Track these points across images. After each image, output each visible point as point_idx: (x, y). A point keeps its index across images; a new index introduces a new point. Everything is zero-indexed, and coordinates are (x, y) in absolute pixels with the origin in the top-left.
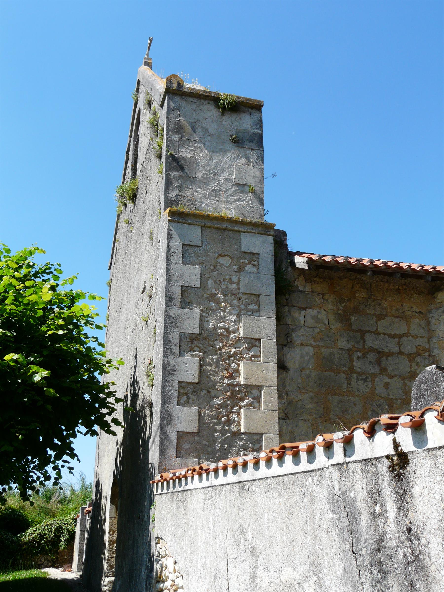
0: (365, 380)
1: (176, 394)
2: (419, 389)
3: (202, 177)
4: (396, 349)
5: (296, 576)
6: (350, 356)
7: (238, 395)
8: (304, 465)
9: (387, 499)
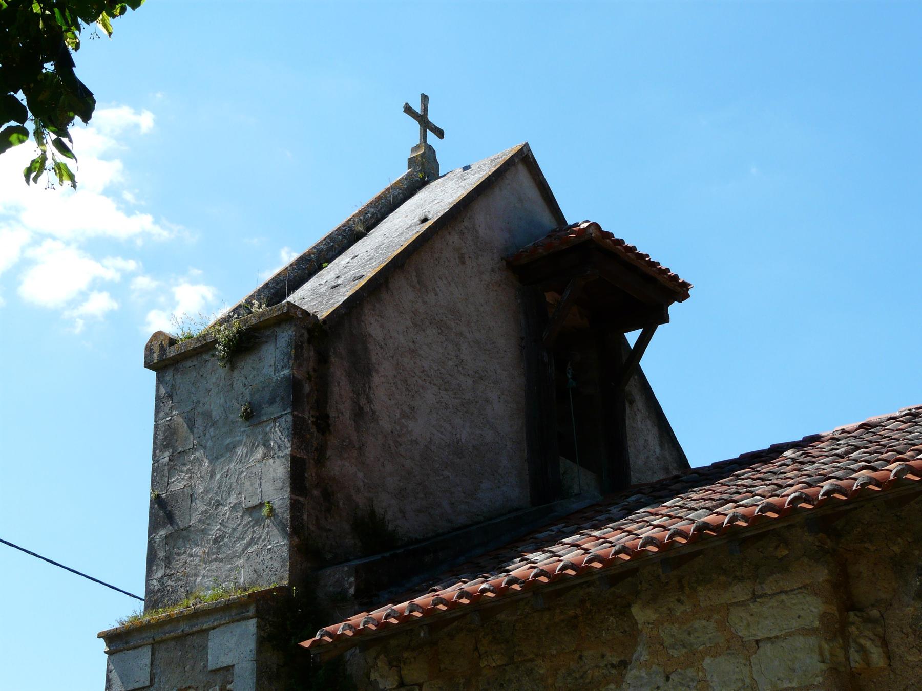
3: (200, 521)
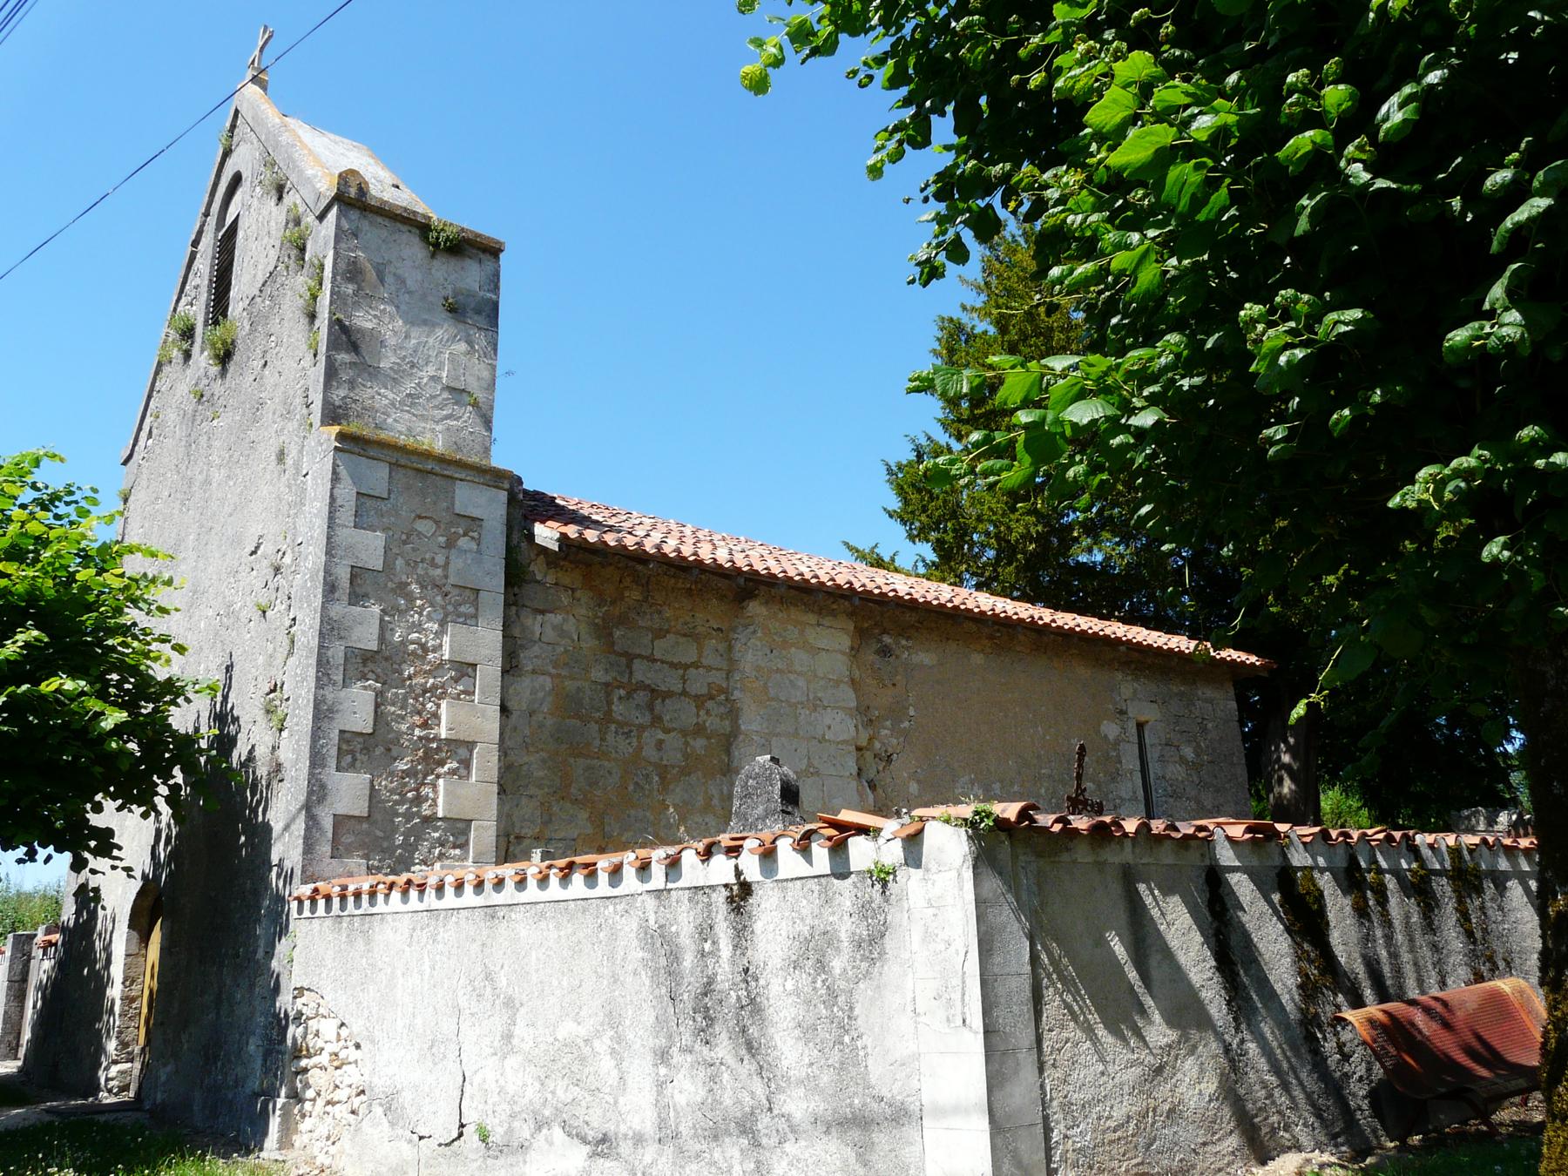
0: (628, 735)
1: (334, 752)
2: (745, 786)
4: (678, 688)
5: (583, 1031)
6: (608, 694)
7: (433, 756)
8: (603, 886)
9: (722, 935)
